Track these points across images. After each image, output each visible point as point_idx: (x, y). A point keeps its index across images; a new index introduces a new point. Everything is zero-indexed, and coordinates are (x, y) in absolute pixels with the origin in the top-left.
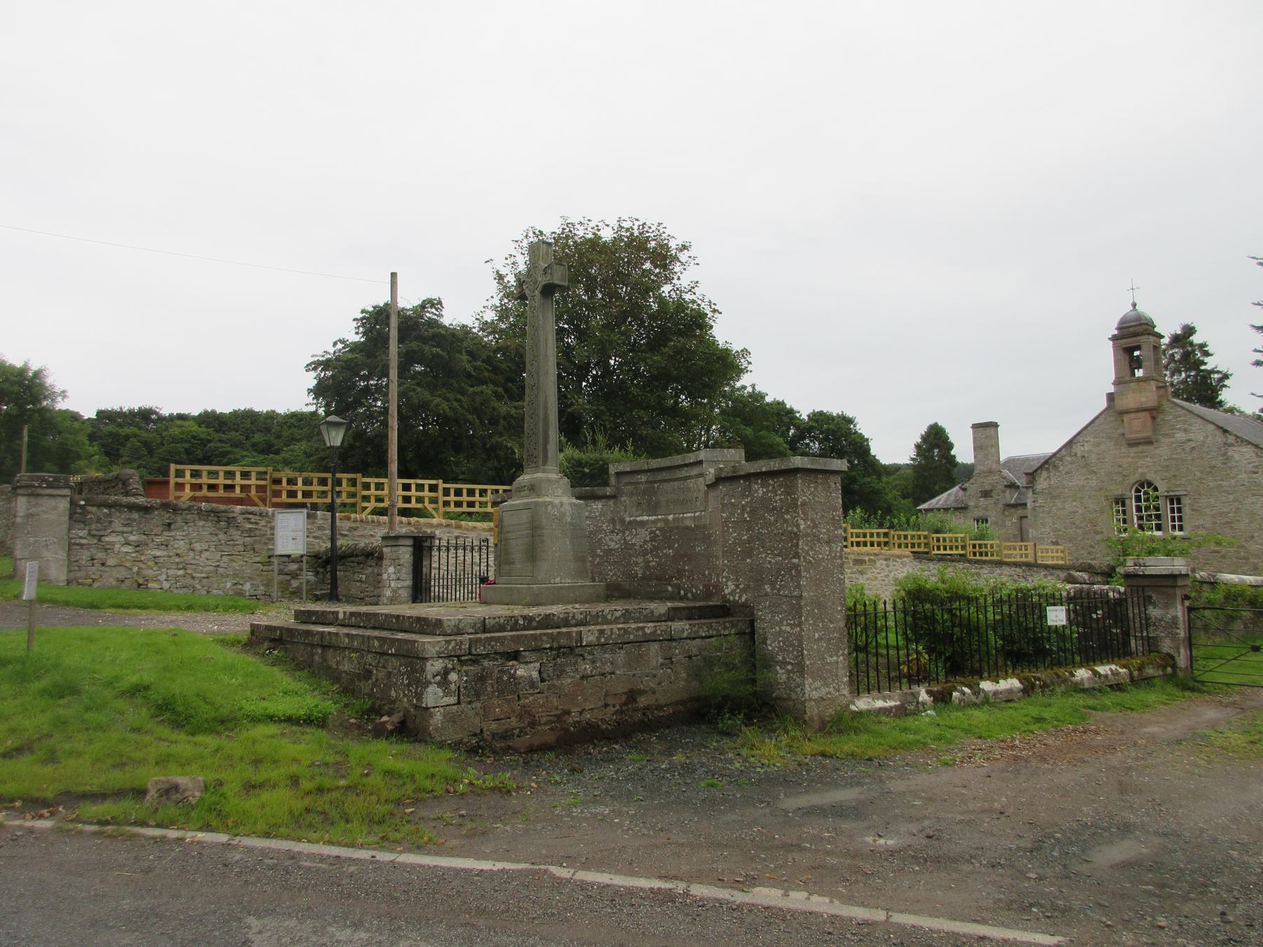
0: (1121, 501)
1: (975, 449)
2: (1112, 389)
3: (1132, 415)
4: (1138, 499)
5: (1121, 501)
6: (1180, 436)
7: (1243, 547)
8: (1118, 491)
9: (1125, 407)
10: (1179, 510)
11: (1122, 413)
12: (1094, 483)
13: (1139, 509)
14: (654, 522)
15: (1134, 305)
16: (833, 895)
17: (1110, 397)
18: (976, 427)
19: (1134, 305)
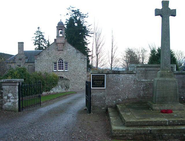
0: (55, 63)
1: (18, 48)
2: (56, 38)
3: (60, 44)
4: (59, 63)
5: (55, 63)
6: (68, 50)
7: (78, 73)
8: (55, 61)
9: (58, 42)
10: (67, 66)
11: (57, 44)
12: (50, 59)
13: (59, 65)
14: (147, 81)
15: (61, 20)
16: (174, 69)
17: (55, 40)
18: (19, 43)
19: (61, 20)
